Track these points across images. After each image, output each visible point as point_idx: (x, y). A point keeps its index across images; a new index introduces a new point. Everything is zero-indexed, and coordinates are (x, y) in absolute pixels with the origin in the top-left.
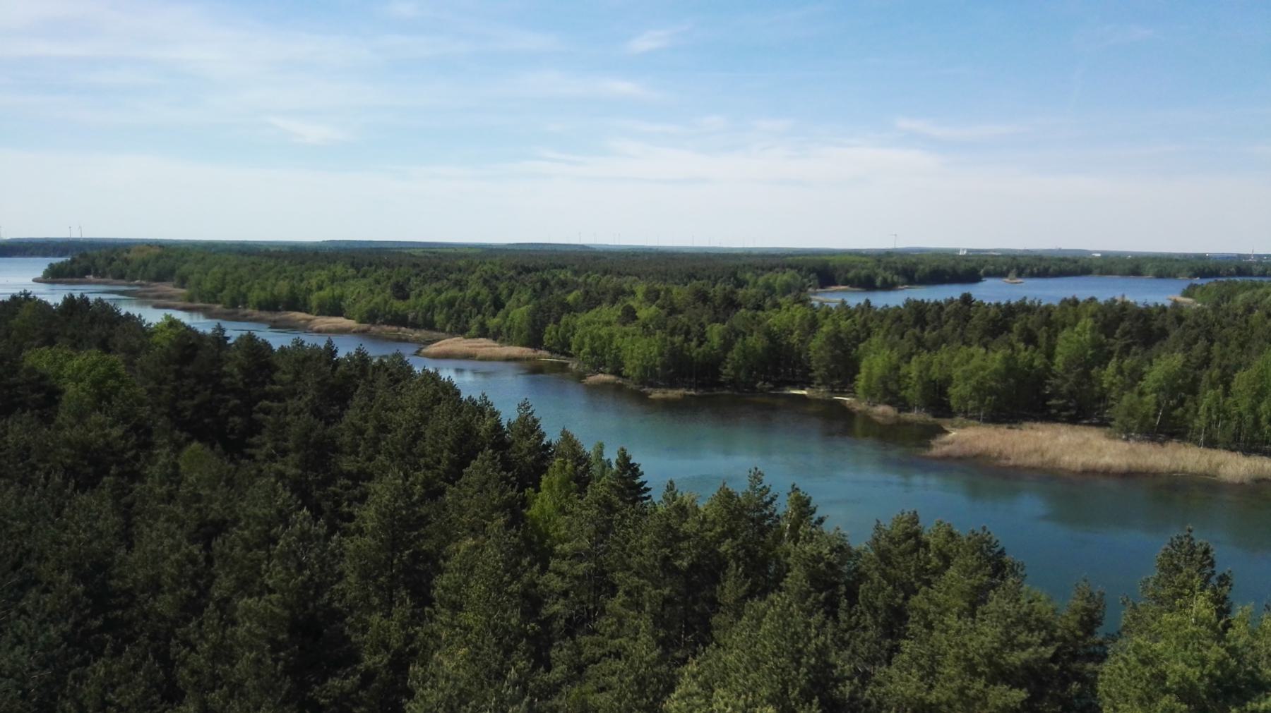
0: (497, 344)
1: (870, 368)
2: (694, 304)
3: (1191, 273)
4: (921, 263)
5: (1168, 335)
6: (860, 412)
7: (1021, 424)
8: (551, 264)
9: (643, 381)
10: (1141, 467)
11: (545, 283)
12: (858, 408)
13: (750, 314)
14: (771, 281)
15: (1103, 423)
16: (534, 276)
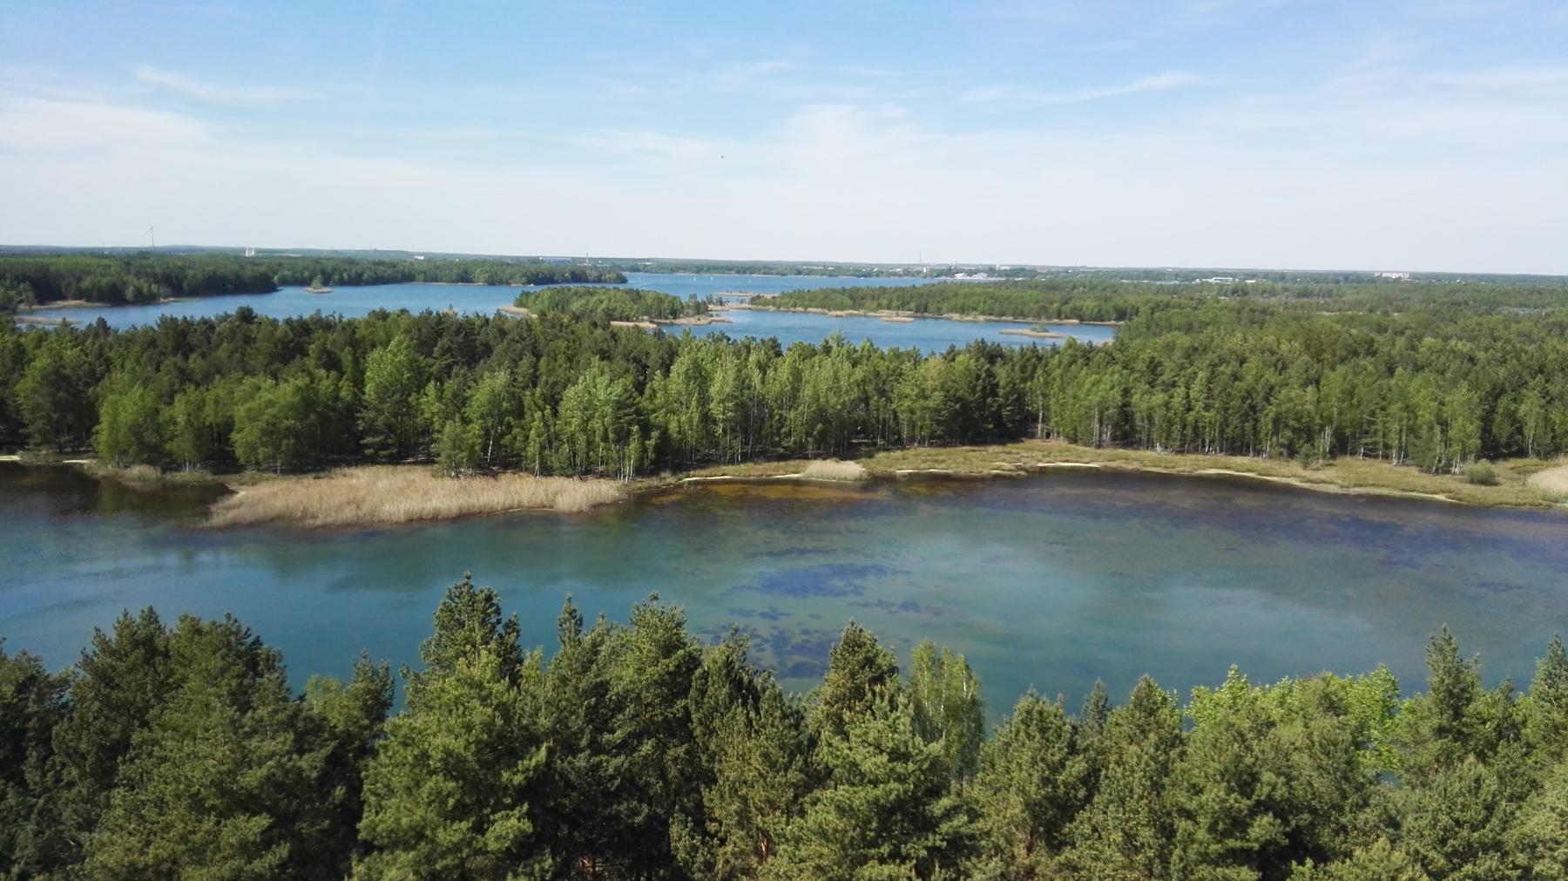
1: (115, 417)
3: (524, 279)
4: (190, 267)
5: (491, 352)
6: (103, 477)
7: (330, 472)
12: (101, 473)
15: (430, 461)
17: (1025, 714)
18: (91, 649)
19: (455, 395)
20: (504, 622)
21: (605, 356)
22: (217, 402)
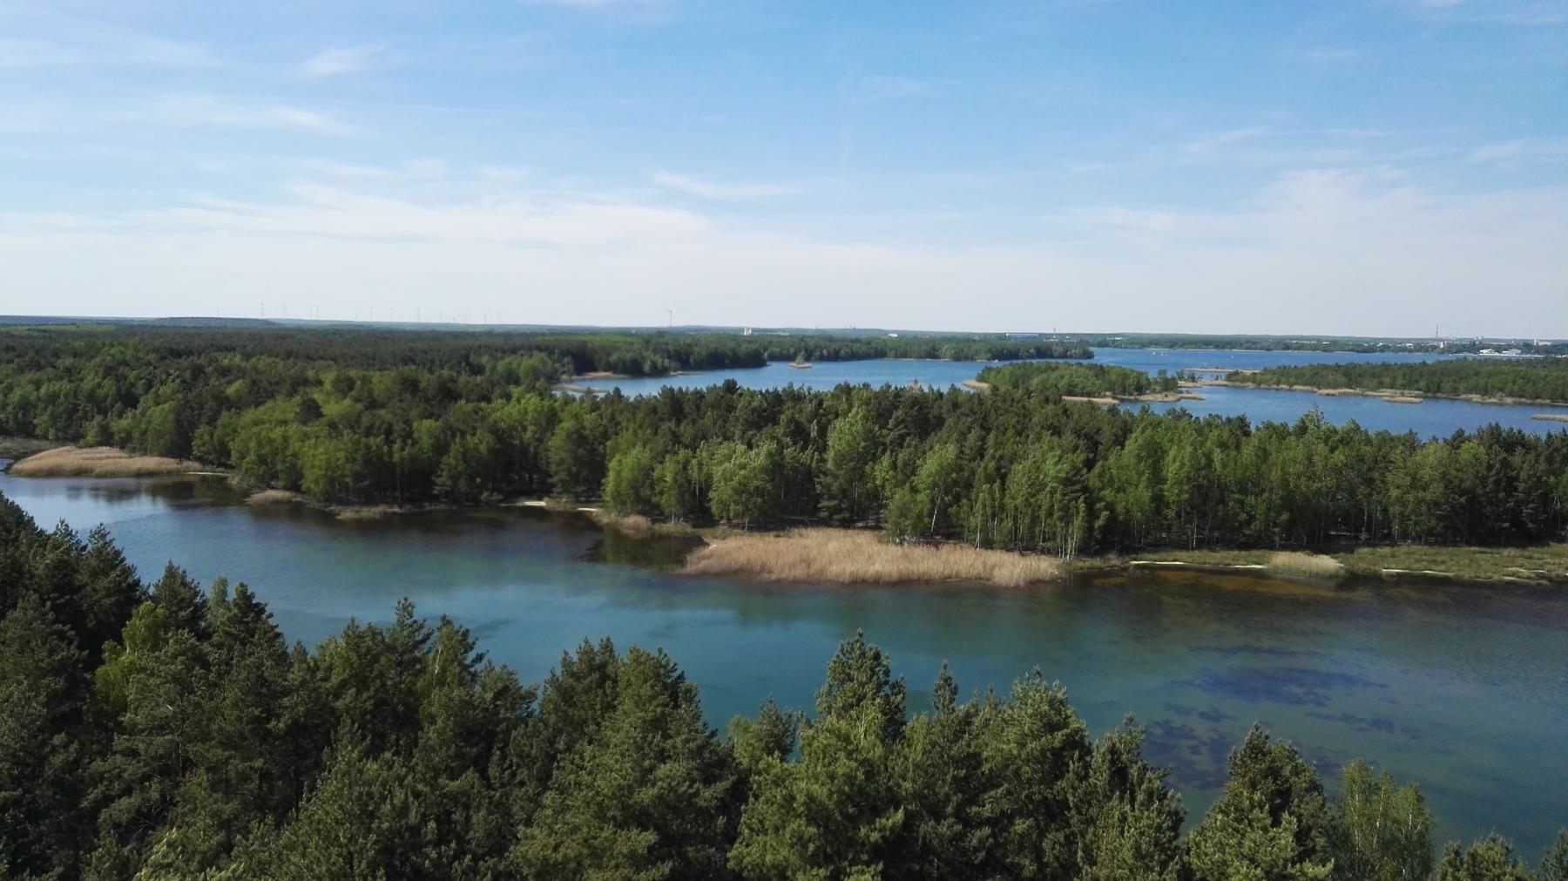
0: (125, 455)
2: (400, 395)
3: (989, 355)
4: (696, 345)
6: (608, 524)
8: (212, 345)
9: (329, 498)
10: (913, 573)
11: (198, 372)
12: (605, 520)
13: (470, 407)
14: (514, 366)
15: (877, 528)
16: (185, 362)
17: (1453, 855)
18: (559, 671)
19: (906, 464)
20: (891, 683)
21: (1057, 431)
22: (700, 464)
